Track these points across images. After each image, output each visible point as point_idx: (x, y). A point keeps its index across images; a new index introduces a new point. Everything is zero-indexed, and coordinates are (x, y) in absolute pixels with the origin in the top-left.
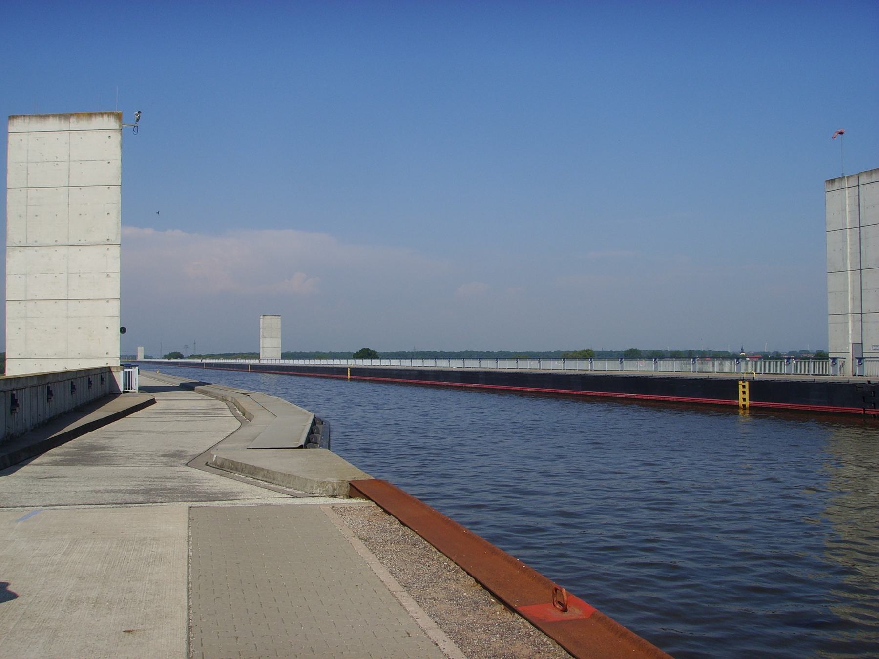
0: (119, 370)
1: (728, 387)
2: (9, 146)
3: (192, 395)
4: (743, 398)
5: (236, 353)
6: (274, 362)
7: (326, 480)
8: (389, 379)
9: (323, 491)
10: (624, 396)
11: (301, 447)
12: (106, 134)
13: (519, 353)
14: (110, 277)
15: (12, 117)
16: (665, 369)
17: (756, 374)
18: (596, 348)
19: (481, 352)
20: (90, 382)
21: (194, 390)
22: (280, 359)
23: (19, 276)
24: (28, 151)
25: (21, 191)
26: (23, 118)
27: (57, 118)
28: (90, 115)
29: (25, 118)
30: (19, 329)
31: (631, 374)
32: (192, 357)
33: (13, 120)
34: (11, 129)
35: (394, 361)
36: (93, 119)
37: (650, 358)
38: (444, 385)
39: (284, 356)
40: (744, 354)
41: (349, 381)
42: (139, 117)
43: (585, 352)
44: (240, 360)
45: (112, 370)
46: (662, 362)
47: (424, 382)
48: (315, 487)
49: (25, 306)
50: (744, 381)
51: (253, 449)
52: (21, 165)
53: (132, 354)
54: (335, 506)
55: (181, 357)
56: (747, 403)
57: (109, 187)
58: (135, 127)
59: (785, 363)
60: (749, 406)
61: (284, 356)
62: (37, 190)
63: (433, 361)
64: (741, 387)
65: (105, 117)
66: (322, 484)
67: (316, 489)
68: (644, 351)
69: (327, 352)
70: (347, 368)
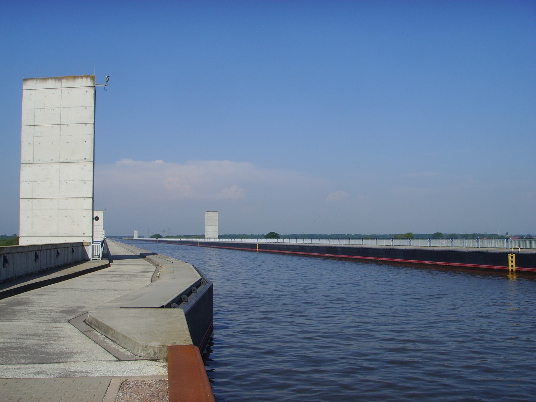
0: (89, 245)
1: (502, 258)
2: (23, 98)
3: (142, 262)
4: (512, 265)
5: (194, 235)
6: (213, 240)
7: (149, 344)
8: (282, 251)
9: (146, 354)
10: (431, 263)
11: (163, 307)
12: (86, 89)
13: (368, 235)
14: (86, 183)
15: (25, 80)
16: (459, 245)
17: (520, 249)
18: (415, 232)
19: (344, 235)
20: (58, 253)
21: (145, 258)
22: (217, 239)
23: (29, 183)
24: (35, 101)
25: (30, 127)
26: (32, 80)
27: (54, 80)
28: (75, 78)
29: (34, 80)
30: (28, 217)
31: (436, 249)
32: (167, 237)
33: (26, 82)
34: (25, 87)
35: (285, 240)
36: (77, 80)
37: (448, 238)
38: (316, 255)
39: (220, 237)
40: (508, 236)
41: (258, 253)
42: (108, 79)
43: (408, 235)
44: (193, 239)
45: (84, 245)
46: (456, 241)
47: (304, 253)
48: (140, 351)
49: (32, 202)
50: (512, 253)
51: (125, 308)
52: (30, 111)
53: (129, 235)
54: (129, 380)
55: (161, 237)
56: (514, 268)
57: (86, 124)
58: (106, 86)
59: (506, 241)
60: (516, 270)
61: (220, 237)
62: (40, 127)
63: (310, 240)
64: (510, 258)
65: (84, 79)
66: (146, 348)
67: (141, 352)
68: (445, 234)
69: (250, 234)
70: (256, 244)
